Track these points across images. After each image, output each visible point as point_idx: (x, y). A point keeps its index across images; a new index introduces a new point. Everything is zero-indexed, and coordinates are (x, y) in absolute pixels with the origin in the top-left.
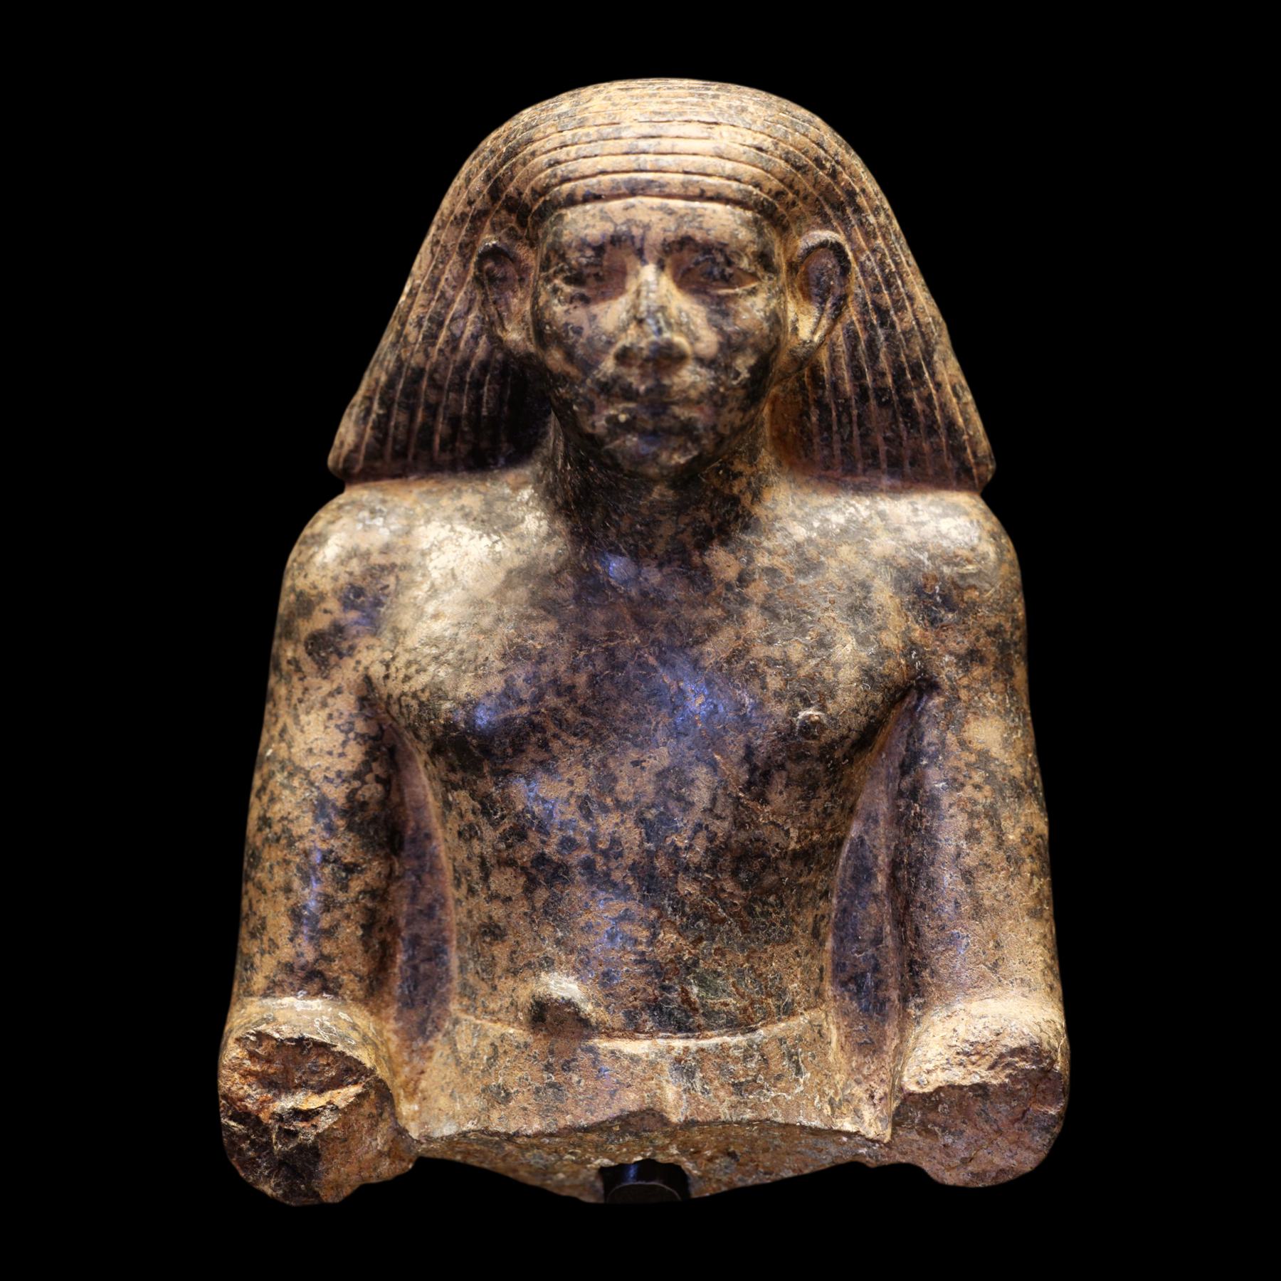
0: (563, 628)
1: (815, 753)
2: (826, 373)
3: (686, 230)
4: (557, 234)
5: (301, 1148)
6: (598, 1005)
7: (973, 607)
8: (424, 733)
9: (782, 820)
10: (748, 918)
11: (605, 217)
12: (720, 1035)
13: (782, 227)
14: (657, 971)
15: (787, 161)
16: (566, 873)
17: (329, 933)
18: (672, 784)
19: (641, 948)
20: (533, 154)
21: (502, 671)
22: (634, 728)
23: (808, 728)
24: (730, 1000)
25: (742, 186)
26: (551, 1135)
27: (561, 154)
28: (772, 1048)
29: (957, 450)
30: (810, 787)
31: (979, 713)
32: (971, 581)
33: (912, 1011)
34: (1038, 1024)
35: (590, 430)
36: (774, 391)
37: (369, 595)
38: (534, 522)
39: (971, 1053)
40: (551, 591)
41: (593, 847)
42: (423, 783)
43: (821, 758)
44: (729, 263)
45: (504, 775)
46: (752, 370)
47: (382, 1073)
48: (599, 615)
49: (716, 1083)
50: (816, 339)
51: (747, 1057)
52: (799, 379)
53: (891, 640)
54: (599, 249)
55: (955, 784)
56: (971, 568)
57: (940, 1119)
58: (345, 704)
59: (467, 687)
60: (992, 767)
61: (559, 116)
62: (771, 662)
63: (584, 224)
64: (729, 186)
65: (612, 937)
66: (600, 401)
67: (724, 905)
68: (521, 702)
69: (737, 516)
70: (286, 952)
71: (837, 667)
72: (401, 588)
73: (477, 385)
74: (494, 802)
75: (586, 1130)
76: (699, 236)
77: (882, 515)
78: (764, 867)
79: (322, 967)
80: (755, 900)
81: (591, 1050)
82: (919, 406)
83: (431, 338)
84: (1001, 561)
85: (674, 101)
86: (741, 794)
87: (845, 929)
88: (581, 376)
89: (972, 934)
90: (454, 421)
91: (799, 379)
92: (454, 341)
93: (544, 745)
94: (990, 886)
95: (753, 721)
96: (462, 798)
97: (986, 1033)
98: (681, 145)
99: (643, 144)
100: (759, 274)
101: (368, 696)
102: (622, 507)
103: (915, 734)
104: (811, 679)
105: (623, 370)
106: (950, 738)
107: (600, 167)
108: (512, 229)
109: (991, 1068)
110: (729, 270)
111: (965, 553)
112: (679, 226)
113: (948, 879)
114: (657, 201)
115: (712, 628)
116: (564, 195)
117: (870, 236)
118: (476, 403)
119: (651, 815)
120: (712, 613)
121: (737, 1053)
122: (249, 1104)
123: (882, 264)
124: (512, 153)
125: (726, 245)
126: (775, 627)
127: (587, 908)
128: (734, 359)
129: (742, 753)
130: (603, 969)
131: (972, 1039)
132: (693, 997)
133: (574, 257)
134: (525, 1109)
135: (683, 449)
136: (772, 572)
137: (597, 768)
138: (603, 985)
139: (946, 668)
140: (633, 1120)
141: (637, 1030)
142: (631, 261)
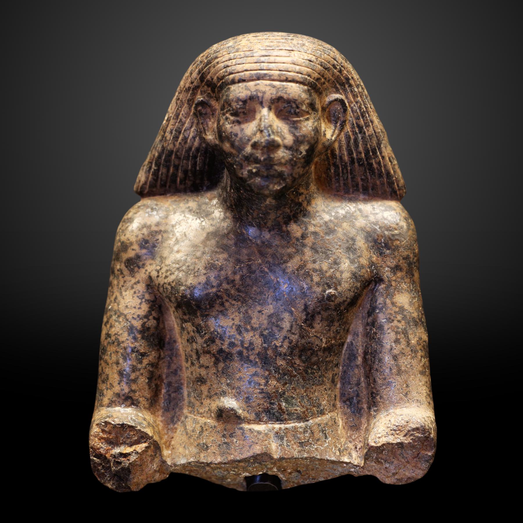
0: (230, 256)
1: (333, 307)
2: (337, 152)
3: (280, 94)
4: (228, 96)
5: (123, 469)
6: (244, 410)
7: (397, 248)
8: (173, 299)
9: (319, 335)
10: (305, 375)
11: (247, 89)
12: (294, 423)
13: (319, 93)
14: (268, 396)
15: (321, 66)
16: (231, 356)
17: (135, 381)
18: (275, 320)
19: (262, 387)
20: (218, 63)
21: (205, 274)
22: (259, 297)
23: (330, 297)
24: (298, 408)
25: (303, 76)
26: (225, 463)
27: (229, 63)
28: (315, 428)
29: (391, 184)
30: (331, 321)
31: (400, 291)
32: (397, 237)
33: (373, 413)
34: (424, 418)
35: (241, 176)
36: (316, 159)
37: (151, 243)
38: (218, 213)
39: (396, 430)
40: (225, 241)
41: (242, 346)
42: (173, 320)
43: (335, 310)
44: (298, 107)
45: (206, 316)
46: (307, 151)
47: (156, 438)
48: (245, 251)
49: (292, 442)
50: (333, 138)
51: (305, 431)
52: (326, 155)
53: (364, 261)
54: (245, 102)
55: (390, 320)
56: (396, 232)
57: (384, 457)
58: (141, 288)
59: (191, 281)
60: (405, 313)
61: (228, 47)
62: (315, 270)
63: (239, 91)
64: (298, 76)
65: (250, 383)
66: (245, 164)
67: (296, 369)
68: (213, 287)
69: (301, 211)
70: (117, 389)
71: (342, 272)
72: (164, 240)
73: (195, 157)
74: (202, 328)
75: (239, 461)
76: (285, 96)
77: (360, 210)
78: (312, 354)
79: (131, 395)
80: (308, 368)
81: (241, 429)
82: (375, 166)
83: (176, 138)
84: (408, 229)
85: (275, 41)
86: (302, 324)
87: (345, 379)
88: (237, 153)
89: (397, 382)
90: (185, 172)
91: (326, 155)
92: (185, 139)
93: (222, 304)
94: (404, 362)
95: (308, 294)
96: (188, 326)
97: (403, 422)
98: (278, 59)
99: (263, 59)
100: (310, 112)
101: (150, 284)
102: (254, 207)
103: (374, 300)
104: (331, 277)
105: (255, 151)
106: (388, 301)
107: (245, 68)
108: (209, 93)
109: (405, 436)
110: (298, 110)
111: (394, 226)
112: (277, 92)
113: (387, 359)
114: (268, 82)
115: (291, 256)
116: (230, 80)
117: (355, 96)
118: (195, 165)
119: (266, 333)
120: (291, 250)
121: (301, 430)
122: (102, 451)
123: (360, 108)
124: (209, 62)
125: (296, 100)
126: (317, 256)
127: (240, 371)
128: (299, 146)
129: (303, 307)
130: (246, 395)
131: (397, 424)
132: (283, 407)
133: (234, 105)
134: (214, 453)
135: (279, 183)
136: (315, 233)
137: (244, 314)
138: (246, 402)
139: (386, 273)
140: (258, 457)
141: (260, 421)
142: (258, 107)
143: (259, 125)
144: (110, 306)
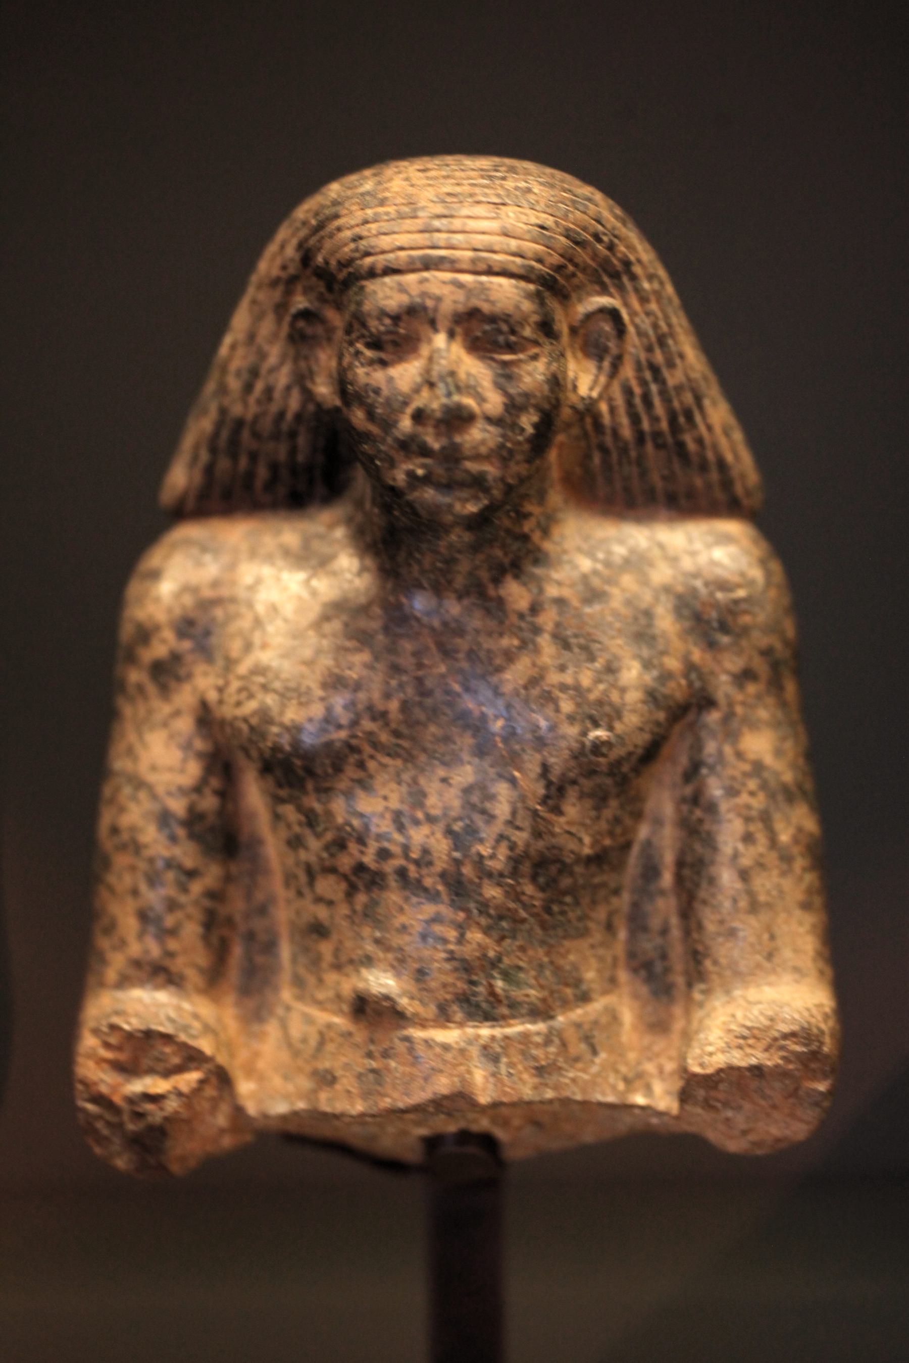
0: (376, 658)
1: (604, 769)
2: (607, 419)
3: (475, 302)
4: (359, 304)
5: (151, 1128)
6: (412, 998)
7: (745, 631)
8: (254, 753)
9: (576, 826)
10: (546, 917)
11: (402, 289)
12: (523, 1023)
13: (563, 296)
14: (465, 967)
15: (567, 237)
16: (383, 880)
17: (173, 932)
18: (477, 800)
19: (451, 947)
20: (339, 229)
21: (322, 699)
22: (441, 748)
23: (598, 747)
24: (532, 992)
25: (526, 262)
26: (373, 1116)
27: (362, 231)
28: (571, 1036)
29: (727, 484)
30: (600, 799)
31: (753, 725)
32: (743, 606)
33: (697, 996)
34: (808, 1010)
35: (391, 483)
36: (560, 438)
37: (199, 628)
38: (347, 562)
39: (748, 1037)
40: (363, 623)
41: (406, 856)
42: (254, 794)
43: (611, 774)
44: (513, 332)
45: (325, 791)
46: (536, 426)
47: (222, 1059)
48: (408, 646)
49: (520, 1067)
50: (595, 394)
51: (548, 1042)
52: (583, 428)
53: (673, 664)
54: (396, 318)
55: (732, 792)
56: (741, 593)
57: (721, 1096)
58: (185, 725)
59: (292, 715)
60: (766, 774)
61: (363, 194)
62: (563, 688)
63: (386, 295)
64: (513, 262)
65: (424, 937)
66: (399, 456)
67: (525, 906)
68: (340, 727)
69: (529, 552)
70: (135, 949)
71: (623, 690)
72: (230, 618)
73: (293, 435)
74: (316, 815)
75: (403, 1111)
76: (486, 308)
77: (661, 546)
78: (560, 872)
79: (167, 963)
80: (552, 901)
81: (407, 1039)
82: (692, 446)
83: (248, 388)
84: (768, 583)
85: (465, 182)
86: (539, 807)
87: (637, 922)
88: (382, 434)
89: (749, 927)
90: (274, 467)
91: (583, 428)
92: (269, 391)
93: (361, 765)
94: (764, 884)
95: (549, 741)
96: (289, 811)
97: (762, 1019)
98: (472, 224)
99: (437, 223)
100: (541, 341)
101: (206, 718)
102: (424, 546)
103: (698, 746)
104: (600, 703)
105: (420, 429)
106: (728, 750)
107: (398, 244)
108: (321, 294)
109: (767, 1050)
110: (513, 338)
111: (736, 579)
112: (468, 298)
113: (727, 877)
114: (448, 276)
115: (510, 657)
116: (366, 269)
117: (644, 300)
118: (293, 451)
119: (458, 827)
120: (506, 642)
121: (538, 1039)
122: (104, 1089)
123: (655, 326)
124: (321, 226)
125: (509, 316)
126: (567, 654)
127: (401, 910)
128: (518, 417)
129: (538, 770)
130: (416, 966)
131: (749, 1024)
132: (499, 991)
133: (374, 325)
134: (349, 1092)
135: (476, 498)
136: (560, 602)
137: (409, 785)
138: (418, 980)
139: (723, 686)
140: (445, 1103)
141: (449, 1021)
142: (425, 329)
143: (428, 371)
144: (120, 764)
